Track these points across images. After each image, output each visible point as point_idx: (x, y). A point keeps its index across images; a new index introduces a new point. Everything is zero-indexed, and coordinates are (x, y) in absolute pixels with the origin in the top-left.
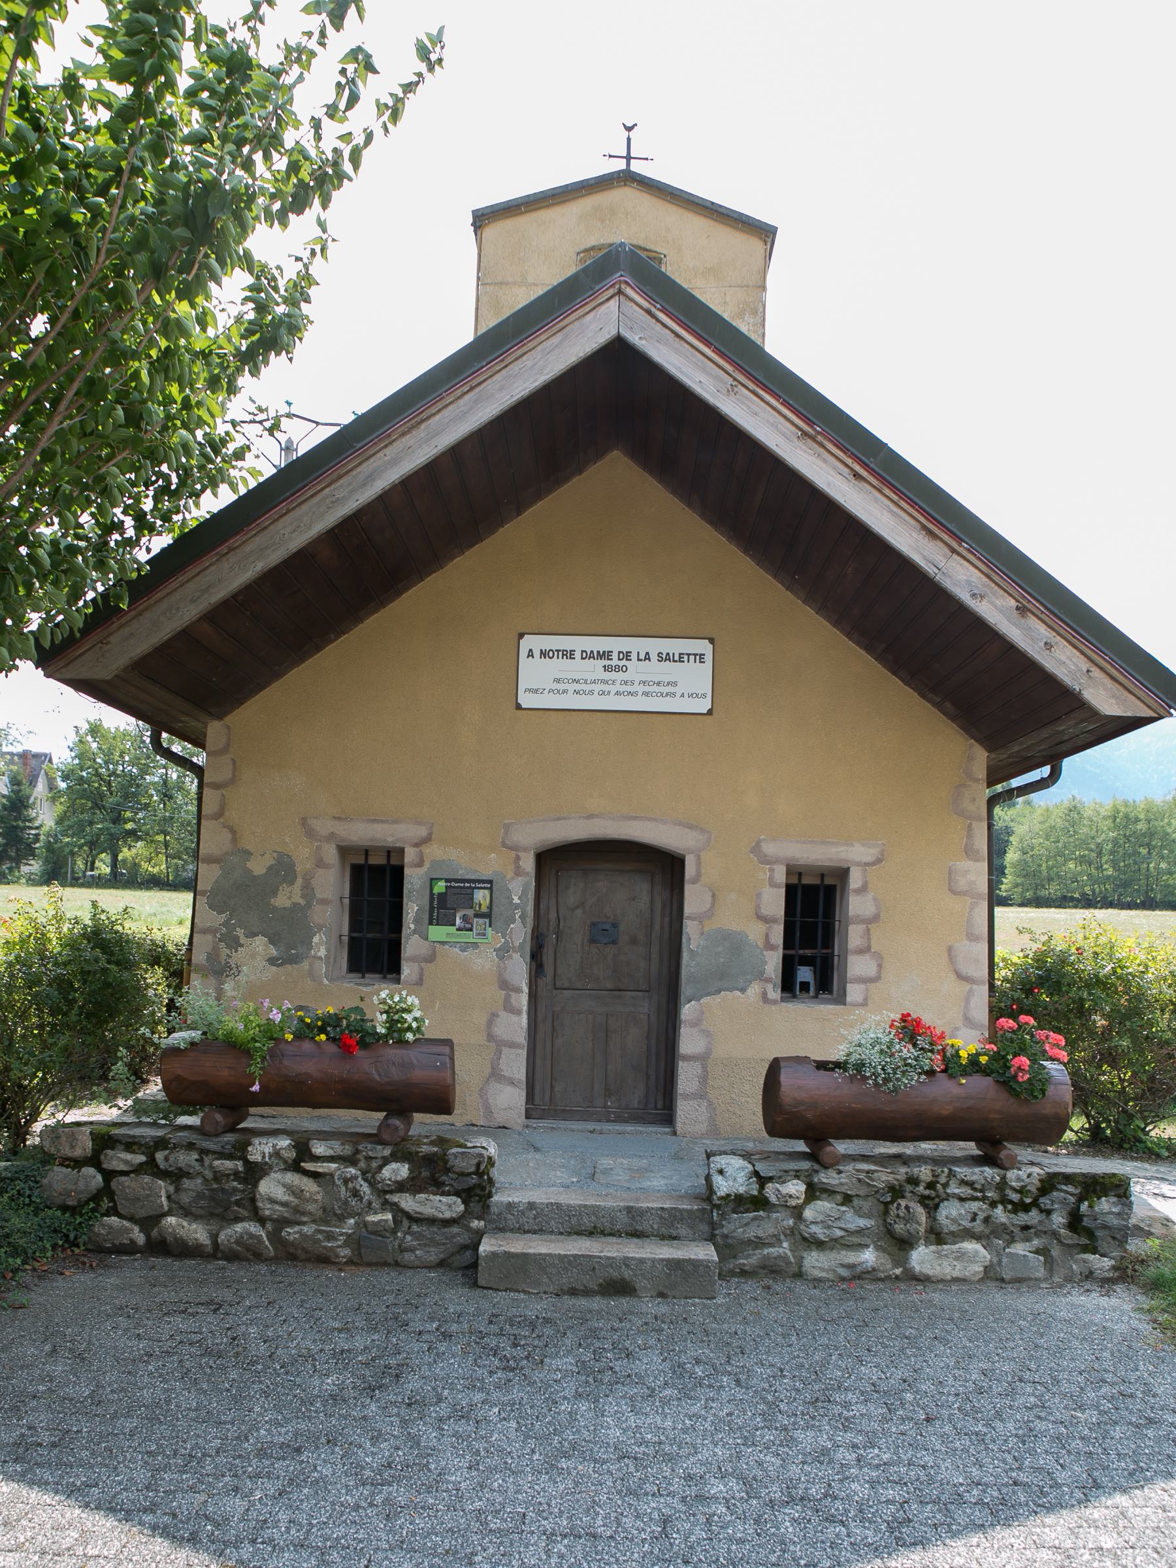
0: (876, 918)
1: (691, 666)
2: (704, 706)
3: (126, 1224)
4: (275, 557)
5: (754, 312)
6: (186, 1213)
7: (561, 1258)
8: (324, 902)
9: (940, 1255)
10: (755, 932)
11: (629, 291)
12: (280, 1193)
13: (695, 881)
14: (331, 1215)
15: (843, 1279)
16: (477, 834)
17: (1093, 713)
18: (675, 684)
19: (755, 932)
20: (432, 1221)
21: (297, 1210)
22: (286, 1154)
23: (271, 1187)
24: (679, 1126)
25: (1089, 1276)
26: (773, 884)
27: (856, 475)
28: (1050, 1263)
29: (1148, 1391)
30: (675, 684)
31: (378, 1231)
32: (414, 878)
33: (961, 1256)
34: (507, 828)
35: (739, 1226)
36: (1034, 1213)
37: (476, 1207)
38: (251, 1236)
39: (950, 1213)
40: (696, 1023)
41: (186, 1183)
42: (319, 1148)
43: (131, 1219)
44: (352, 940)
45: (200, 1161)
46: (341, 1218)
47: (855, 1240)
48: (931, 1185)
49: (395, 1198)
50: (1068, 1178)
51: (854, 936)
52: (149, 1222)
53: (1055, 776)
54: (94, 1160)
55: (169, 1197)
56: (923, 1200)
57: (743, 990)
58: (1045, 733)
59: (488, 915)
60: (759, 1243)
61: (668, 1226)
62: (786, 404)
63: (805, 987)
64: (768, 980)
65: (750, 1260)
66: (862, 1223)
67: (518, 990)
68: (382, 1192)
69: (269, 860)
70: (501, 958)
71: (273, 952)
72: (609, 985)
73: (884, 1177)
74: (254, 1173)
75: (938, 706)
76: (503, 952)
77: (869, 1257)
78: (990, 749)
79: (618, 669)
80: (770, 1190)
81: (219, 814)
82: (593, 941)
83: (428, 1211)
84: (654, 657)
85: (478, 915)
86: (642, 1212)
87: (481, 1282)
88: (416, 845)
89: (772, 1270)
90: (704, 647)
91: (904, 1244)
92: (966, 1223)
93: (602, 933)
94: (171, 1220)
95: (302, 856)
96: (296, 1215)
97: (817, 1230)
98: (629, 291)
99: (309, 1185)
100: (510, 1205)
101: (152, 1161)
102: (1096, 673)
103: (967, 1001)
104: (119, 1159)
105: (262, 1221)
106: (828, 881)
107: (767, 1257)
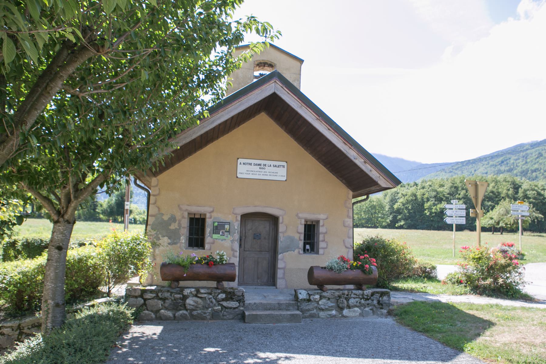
0: (326, 233)
1: (281, 168)
2: (284, 179)
3: (150, 312)
4: (188, 140)
5: (298, 80)
6: (166, 309)
7: (265, 315)
8: (184, 228)
9: (350, 311)
10: (297, 236)
11: (277, 82)
12: (192, 303)
13: (282, 223)
14: (205, 307)
15: (328, 318)
16: (224, 212)
17: (380, 186)
18: (277, 173)
19: (297, 236)
20: (231, 308)
21: (197, 307)
22: (193, 293)
23: (190, 301)
24: (278, 286)
25: (382, 314)
26: (301, 224)
27: (329, 129)
28: (373, 312)
29: (399, 332)
30: (277, 173)
31: (217, 311)
32: (209, 222)
33: (354, 311)
34: (234, 209)
35: (305, 306)
36: (370, 300)
37: (242, 304)
38: (184, 314)
39: (352, 301)
40: (282, 260)
41: (167, 301)
42: (202, 291)
43: (152, 311)
44: (190, 238)
45: (171, 295)
46: (207, 308)
47: (331, 308)
48: (347, 295)
49: (221, 303)
50: (377, 292)
51: (321, 237)
52: (157, 312)
53: (367, 198)
54: (141, 296)
55: (162, 305)
56: (346, 298)
57: (294, 251)
58: (367, 189)
59: (229, 232)
60: (309, 310)
61: (287, 307)
62: (313, 112)
63: (308, 250)
64: (300, 248)
65: (308, 314)
66: (332, 304)
67: (237, 251)
68: (218, 301)
69: (169, 216)
70: (232, 243)
71: (169, 241)
72: (258, 250)
73: (337, 293)
74: (185, 298)
75: (341, 181)
76: (232, 241)
77: (334, 312)
78: (353, 192)
79: (263, 168)
80: (311, 297)
81: (155, 203)
82: (254, 238)
83: (230, 306)
84: (272, 166)
85: (226, 232)
86: (281, 304)
87: (246, 321)
88: (210, 213)
89: (312, 316)
90: (284, 164)
91: (342, 309)
92: (355, 304)
93: (257, 236)
94: (162, 311)
95: (178, 215)
96: (196, 308)
97: (322, 307)
98: (277, 82)
99: (199, 300)
100: (250, 304)
101: (157, 296)
102: (381, 177)
103: (348, 253)
104: (148, 296)
105: (187, 310)
106: (314, 223)
107: (311, 313)
